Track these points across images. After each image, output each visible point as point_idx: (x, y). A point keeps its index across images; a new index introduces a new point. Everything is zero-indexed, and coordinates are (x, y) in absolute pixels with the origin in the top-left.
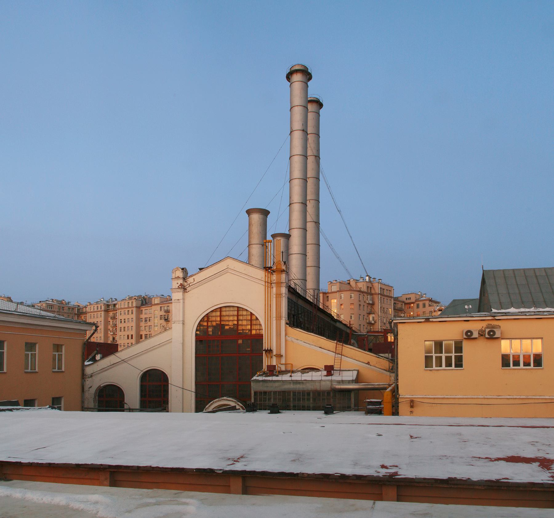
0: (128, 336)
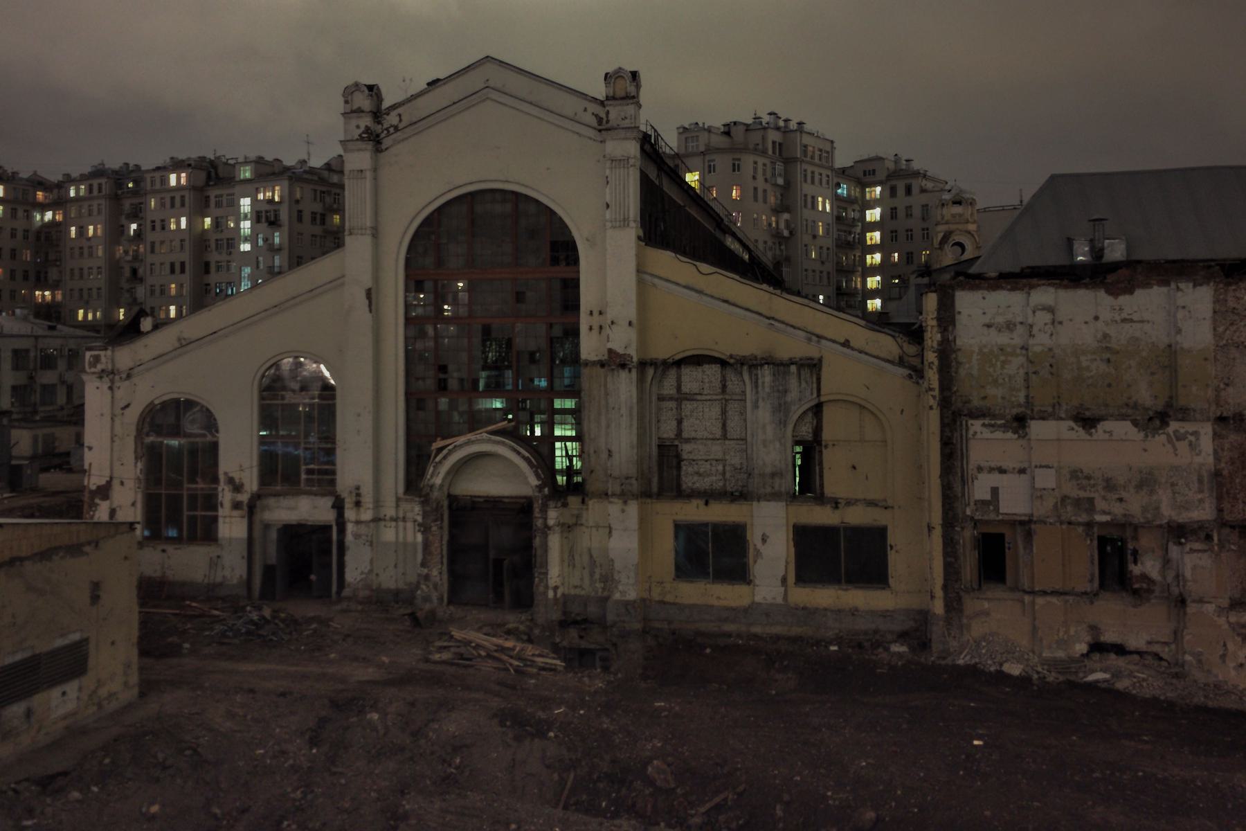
0: (172, 265)
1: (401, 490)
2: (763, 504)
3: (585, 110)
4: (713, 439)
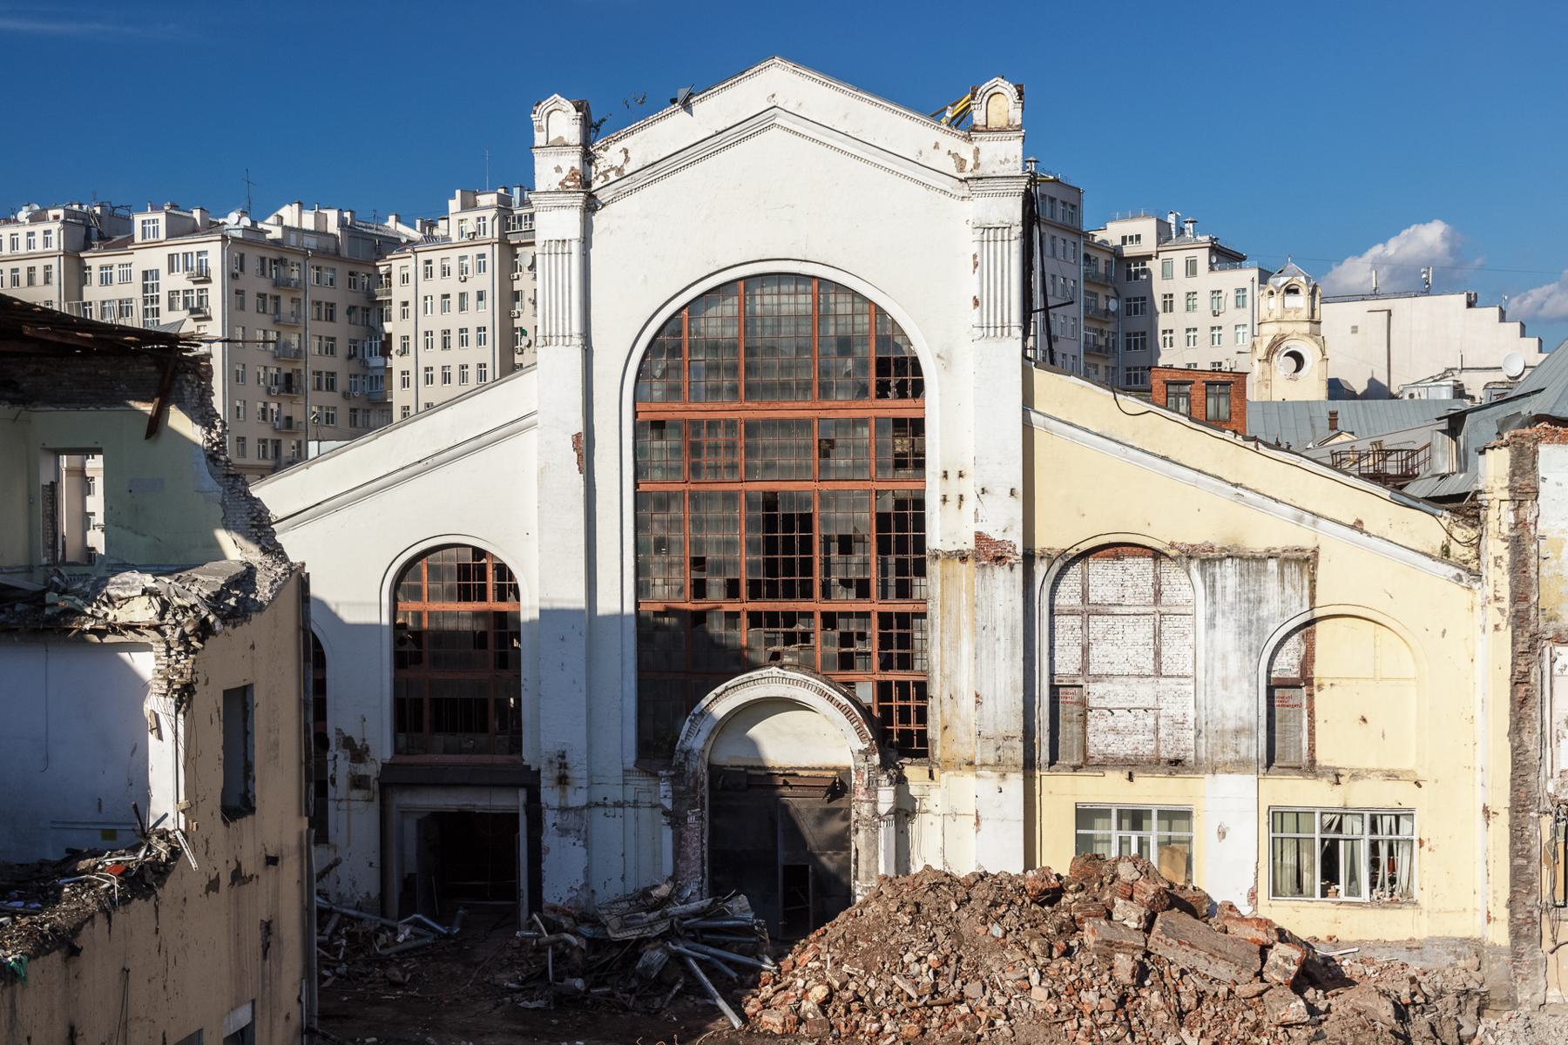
1: (631, 758)
2: (1222, 777)
3: (936, 146)
4: (1139, 676)
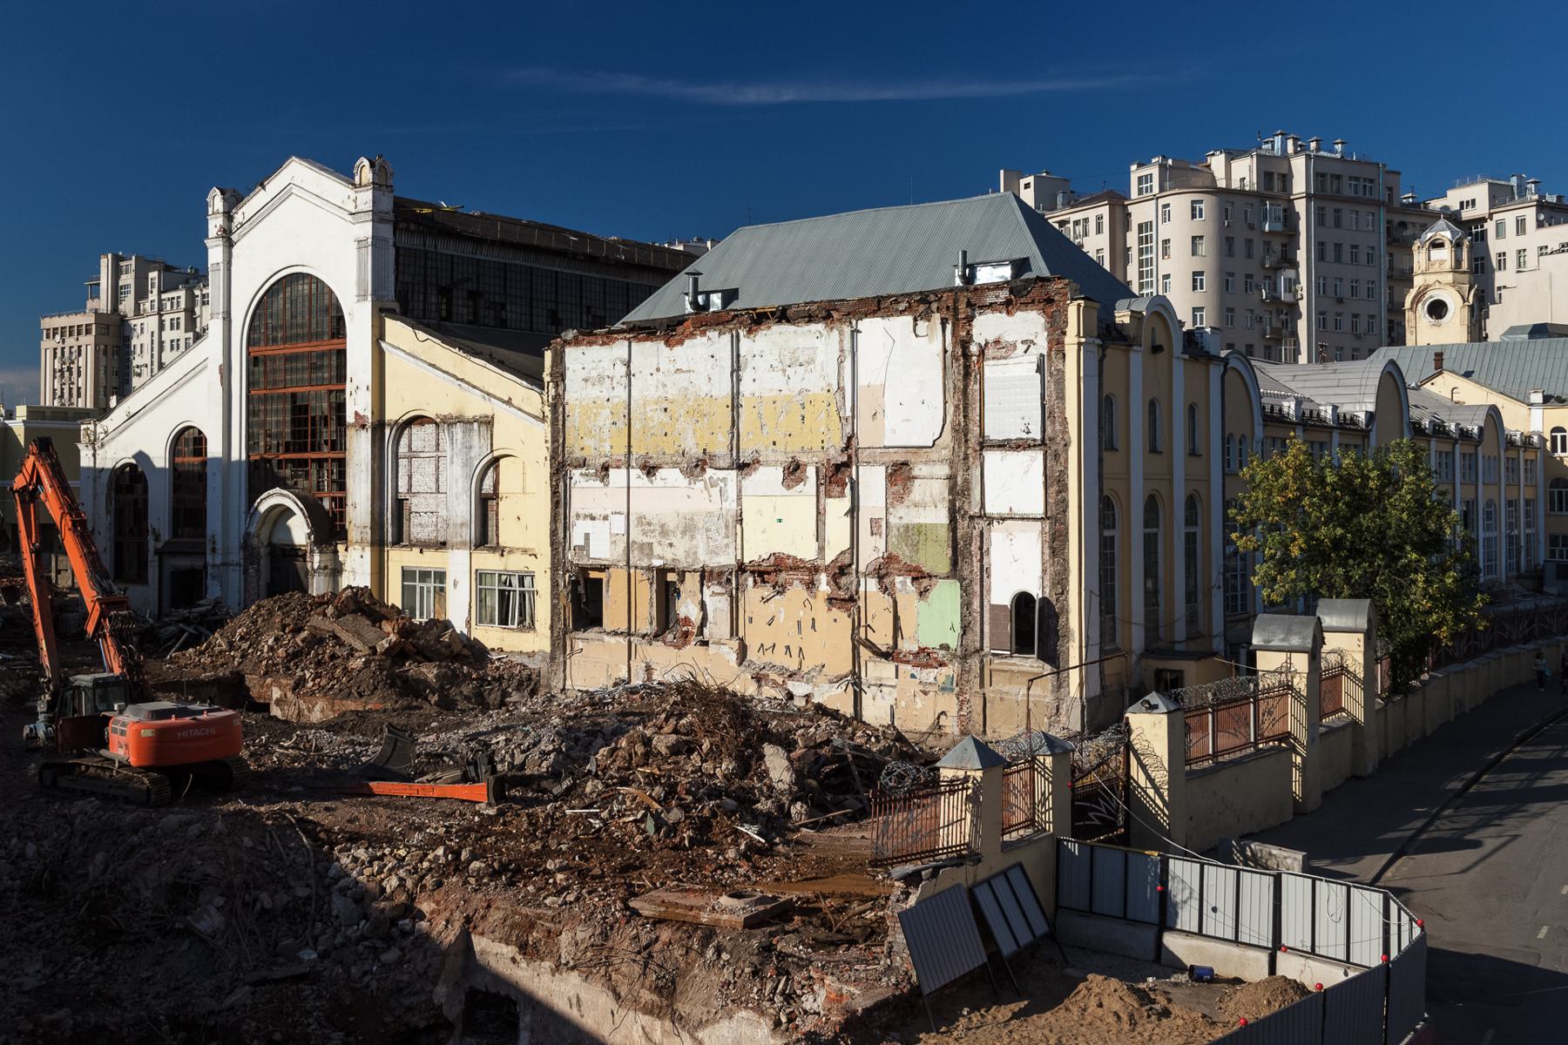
2: (456, 551)
